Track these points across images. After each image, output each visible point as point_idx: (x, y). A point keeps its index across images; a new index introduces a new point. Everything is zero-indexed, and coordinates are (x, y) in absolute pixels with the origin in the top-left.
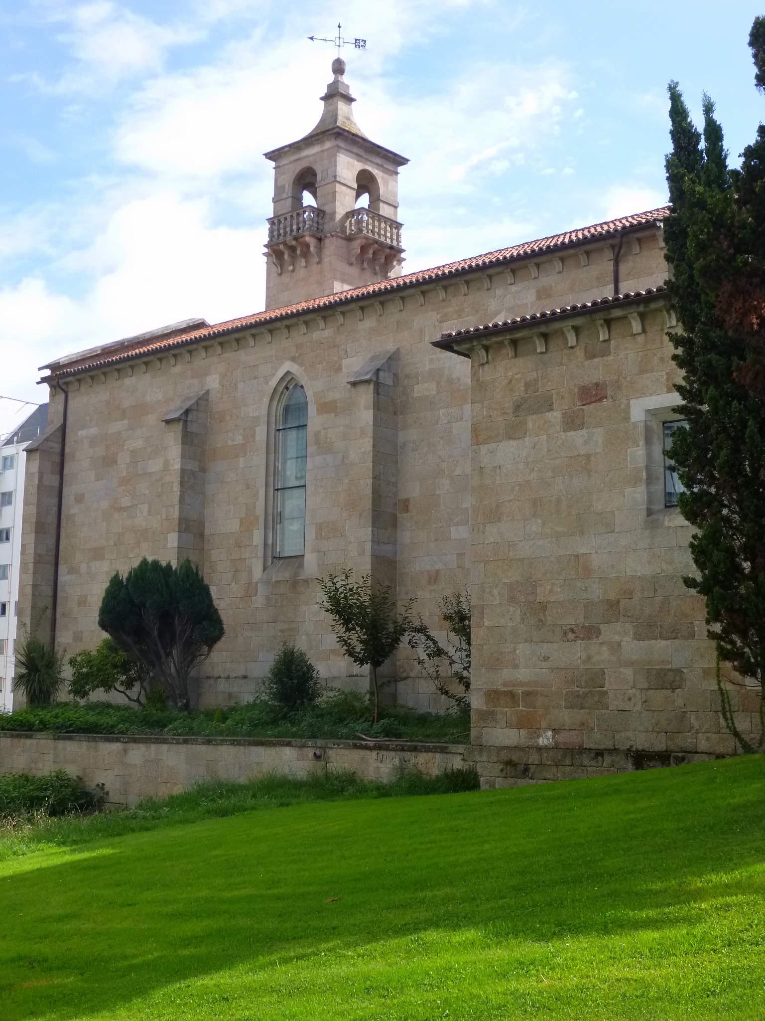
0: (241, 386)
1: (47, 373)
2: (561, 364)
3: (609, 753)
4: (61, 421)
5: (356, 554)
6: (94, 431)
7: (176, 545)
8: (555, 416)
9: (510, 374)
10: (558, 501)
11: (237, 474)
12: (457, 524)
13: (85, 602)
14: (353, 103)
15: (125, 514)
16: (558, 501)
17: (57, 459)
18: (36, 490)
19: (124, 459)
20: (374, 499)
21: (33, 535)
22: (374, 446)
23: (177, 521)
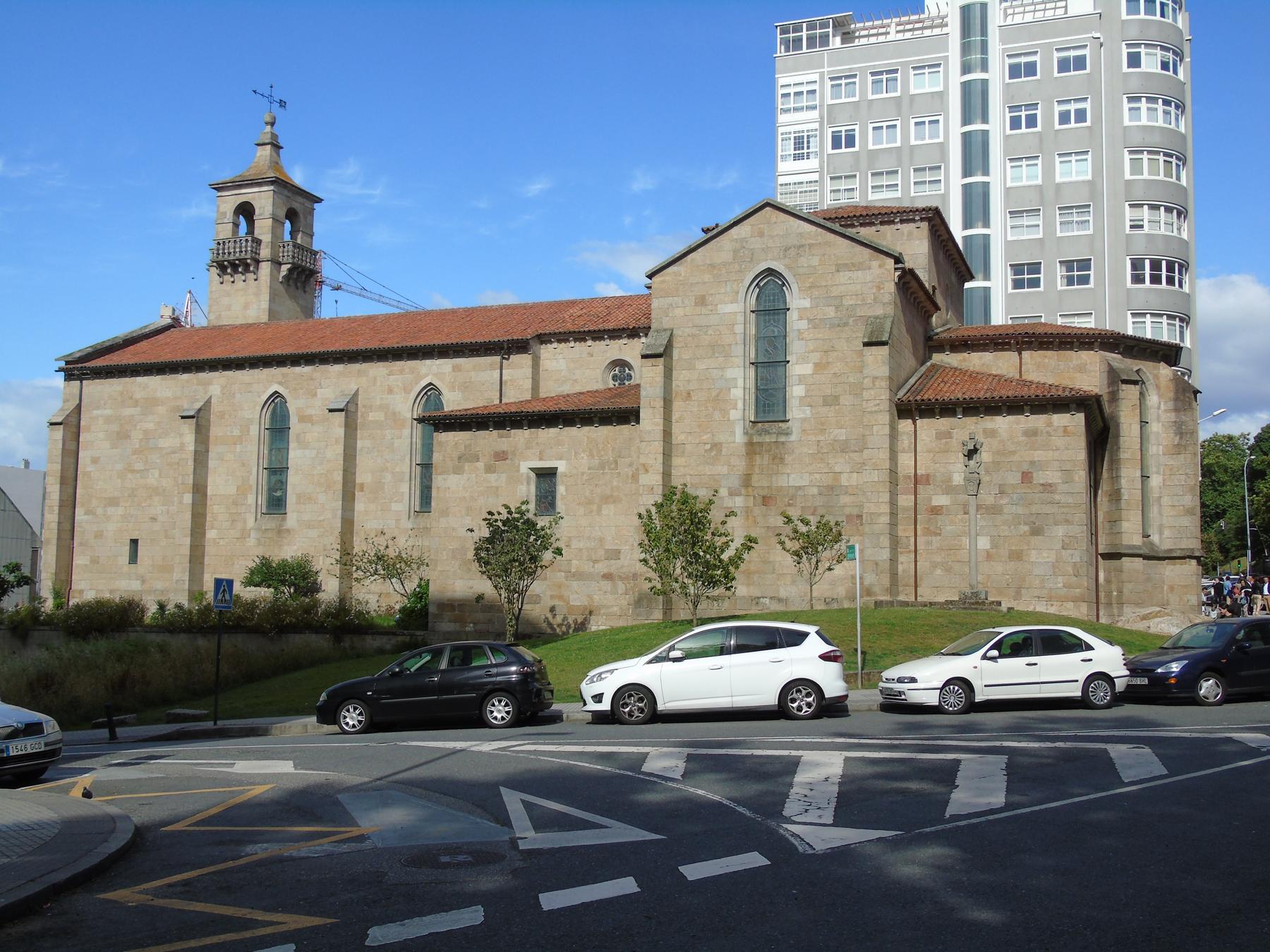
0: (238, 396)
1: (62, 364)
2: (485, 438)
3: (872, 707)
4: (78, 402)
5: (331, 517)
6: (108, 412)
7: (190, 502)
8: (480, 465)
9: (456, 439)
10: (481, 508)
11: (235, 456)
12: (396, 502)
13: (101, 535)
14: (281, 150)
15: (139, 475)
16: (481, 508)
17: (75, 430)
18: (60, 451)
19: (137, 435)
20: (344, 484)
21: (58, 486)
22: (344, 450)
23: (192, 486)
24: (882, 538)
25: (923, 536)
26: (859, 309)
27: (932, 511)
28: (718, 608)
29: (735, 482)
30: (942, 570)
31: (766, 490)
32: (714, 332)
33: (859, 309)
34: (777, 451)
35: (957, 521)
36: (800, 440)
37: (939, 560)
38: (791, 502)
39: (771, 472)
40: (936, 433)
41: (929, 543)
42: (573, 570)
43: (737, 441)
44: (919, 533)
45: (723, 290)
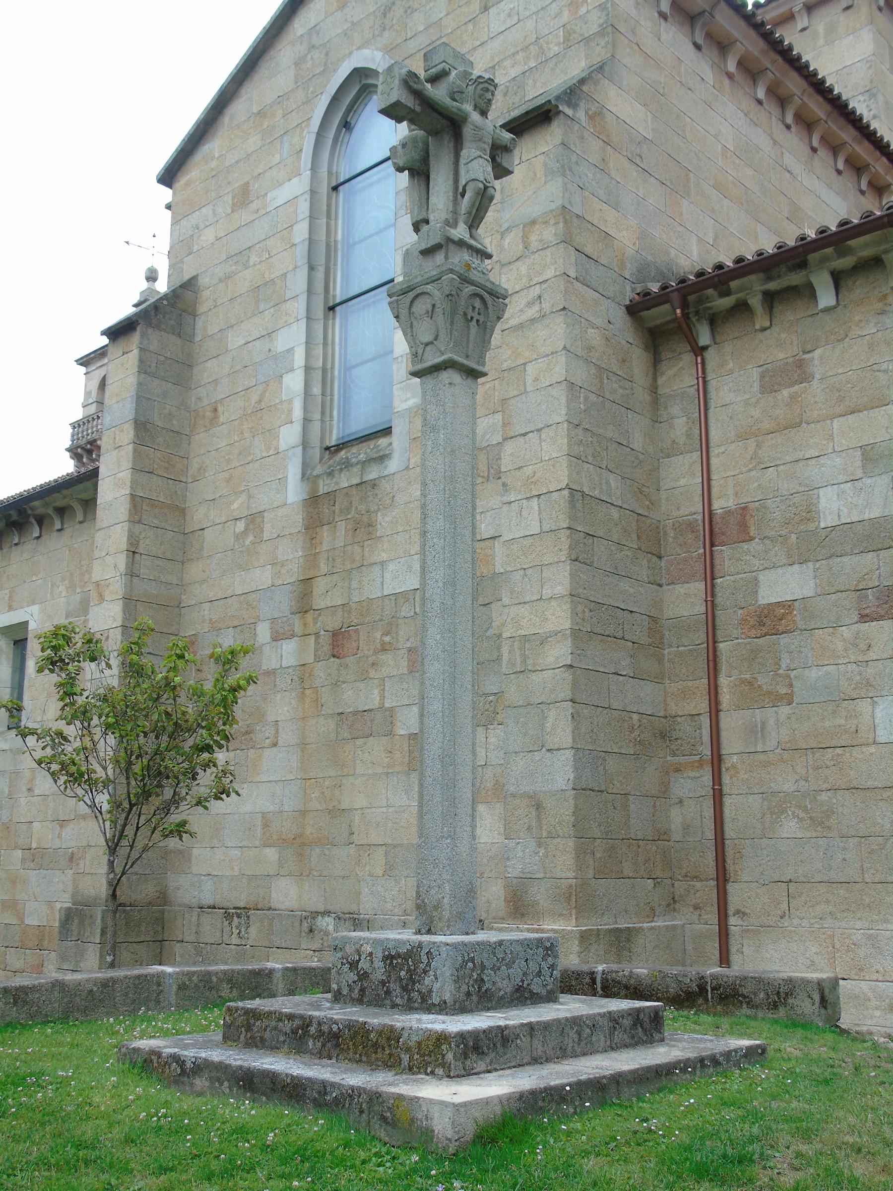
24: (552, 714)
25: (738, 708)
26: (530, 82)
27: (762, 624)
28: (238, 941)
29: (283, 603)
30: (801, 820)
31: (340, 613)
32: (260, 257)
33: (530, 82)
34: (362, 508)
35: (840, 645)
36: (407, 468)
37: (789, 786)
38: (387, 639)
39: (348, 567)
40: (762, 376)
41: (757, 731)
42: (34, 846)
43: (289, 501)
44: (725, 698)
45: (277, 158)
